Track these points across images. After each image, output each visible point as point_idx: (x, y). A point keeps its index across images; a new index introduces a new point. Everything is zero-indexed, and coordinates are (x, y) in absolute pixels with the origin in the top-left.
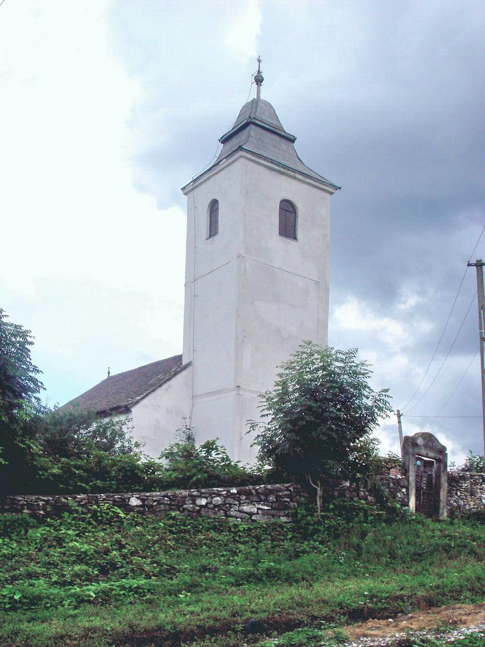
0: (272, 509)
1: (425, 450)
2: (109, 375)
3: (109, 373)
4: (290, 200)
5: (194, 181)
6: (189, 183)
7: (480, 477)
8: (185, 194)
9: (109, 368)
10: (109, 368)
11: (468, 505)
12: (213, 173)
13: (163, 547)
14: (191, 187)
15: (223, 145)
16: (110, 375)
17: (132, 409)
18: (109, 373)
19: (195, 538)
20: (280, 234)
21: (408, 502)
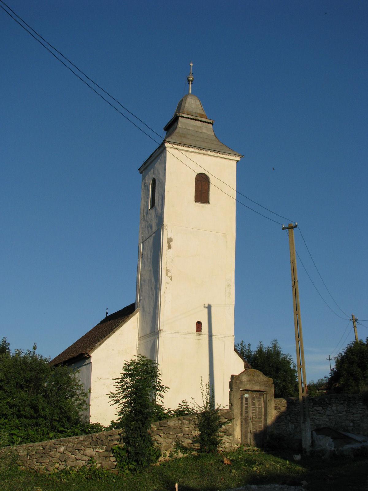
0: (106, 451)
1: (249, 385)
2: (107, 315)
3: (107, 313)
4: (204, 173)
5: (145, 163)
6: (142, 166)
7: (311, 401)
8: (141, 173)
9: (107, 309)
10: (107, 309)
11: (58, 464)
12: (153, 158)
13: (50, 483)
14: (143, 169)
15: (166, 132)
16: (108, 315)
17: (91, 355)
18: (107, 313)
19: (243, 457)
20: (195, 201)
21: (233, 430)
